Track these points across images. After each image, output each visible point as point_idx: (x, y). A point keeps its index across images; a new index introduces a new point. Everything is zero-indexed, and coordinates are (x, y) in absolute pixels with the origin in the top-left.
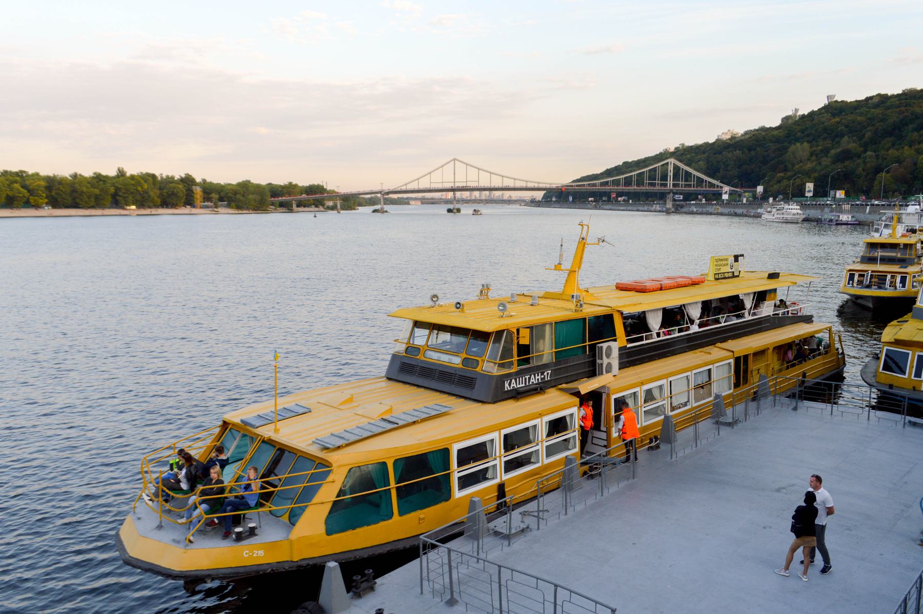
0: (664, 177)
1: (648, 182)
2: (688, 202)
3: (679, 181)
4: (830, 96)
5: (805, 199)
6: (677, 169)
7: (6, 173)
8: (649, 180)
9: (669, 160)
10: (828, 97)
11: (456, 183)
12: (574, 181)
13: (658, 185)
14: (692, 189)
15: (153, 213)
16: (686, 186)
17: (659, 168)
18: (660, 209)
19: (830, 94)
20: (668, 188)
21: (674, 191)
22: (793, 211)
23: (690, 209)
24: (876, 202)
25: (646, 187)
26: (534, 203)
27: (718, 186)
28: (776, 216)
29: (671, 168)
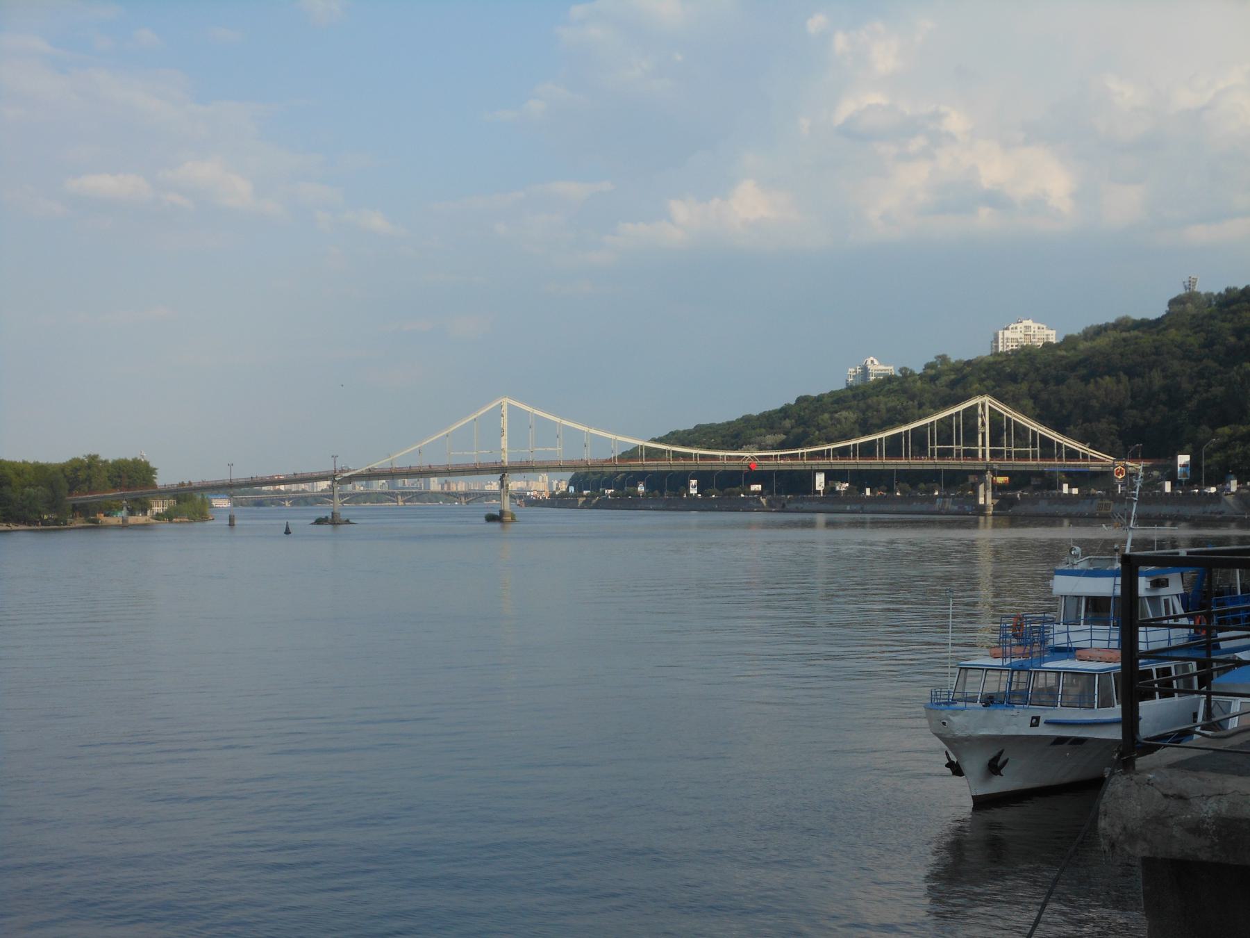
0: (971, 434)
1: (936, 447)
6: (996, 419)
12: (675, 438)
18: (956, 508)
21: (996, 467)
25: (932, 458)
27: (1085, 457)
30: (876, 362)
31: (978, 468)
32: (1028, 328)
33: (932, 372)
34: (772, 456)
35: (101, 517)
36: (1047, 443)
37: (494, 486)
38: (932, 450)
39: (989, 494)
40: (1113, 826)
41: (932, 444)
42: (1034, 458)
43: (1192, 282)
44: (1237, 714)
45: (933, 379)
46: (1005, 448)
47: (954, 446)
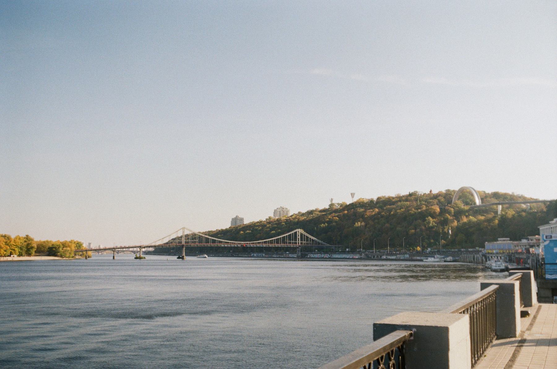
6: (301, 234)
9: (297, 230)
13: (190, 242)
17: (293, 235)
19: (352, 192)
24: (484, 208)
27: (322, 244)
34: (229, 242)
37: (139, 250)
40: (140, 269)
41: (287, 240)
47: (303, 242)
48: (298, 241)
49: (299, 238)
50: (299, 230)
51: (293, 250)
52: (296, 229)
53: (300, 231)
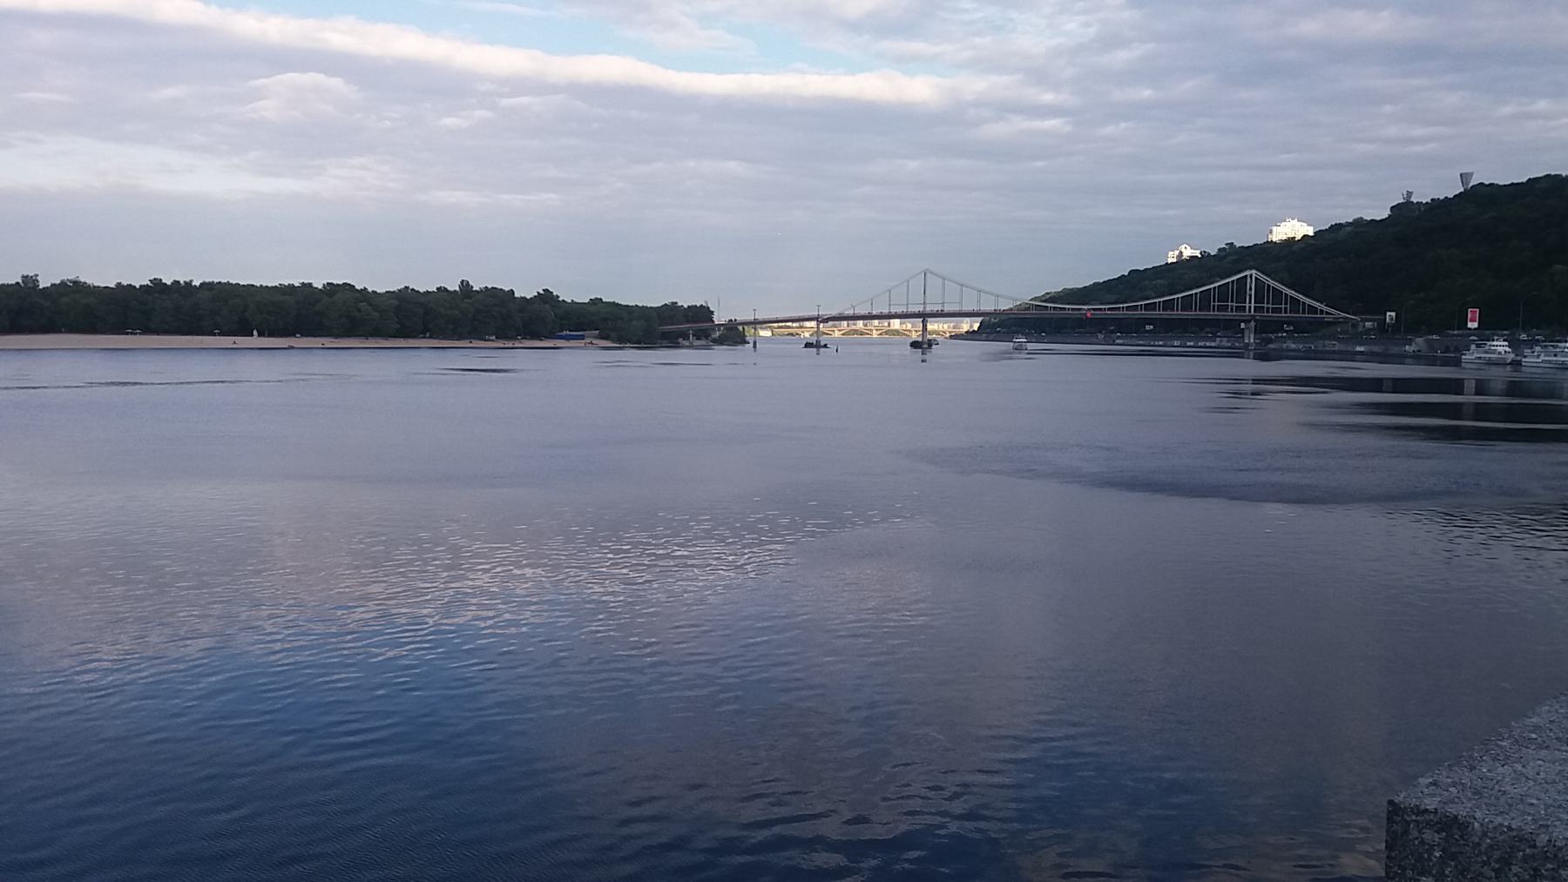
2: (1280, 335)
3: (1228, 302)
4: (1466, 174)
5: (1466, 332)
7: (3, 285)
8: (1218, 302)
9: (1247, 273)
10: (1461, 175)
11: (928, 306)
14: (1265, 314)
15: (516, 345)
16: (1274, 310)
18: (1230, 344)
20: (1247, 313)
21: (1258, 318)
22: (1498, 348)
23: (1285, 345)
25: (1159, 310)
26: (970, 335)
27: (1322, 312)
28: (1542, 358)
29: (1251, 286)
30: (1188, 248)
31: (1246, 318)
32: (1294, 226)
33: (1223, 253)
34: (1047, 307)
35: (680, 340)
36: (1295, 301)
38: (1214, 306)
39: (1252, 336)
41: (1214, 302)
42: (1286, 312)
43: (1410, 194)
44: (104, 687)
45: (1224, 257)
46: (1235, 304)
48: (1248, 301)
49: (1250, 296)
50: (1254, 272)
51: (1231, 327)
52: (1246, 269)
53: (1254, 275)
